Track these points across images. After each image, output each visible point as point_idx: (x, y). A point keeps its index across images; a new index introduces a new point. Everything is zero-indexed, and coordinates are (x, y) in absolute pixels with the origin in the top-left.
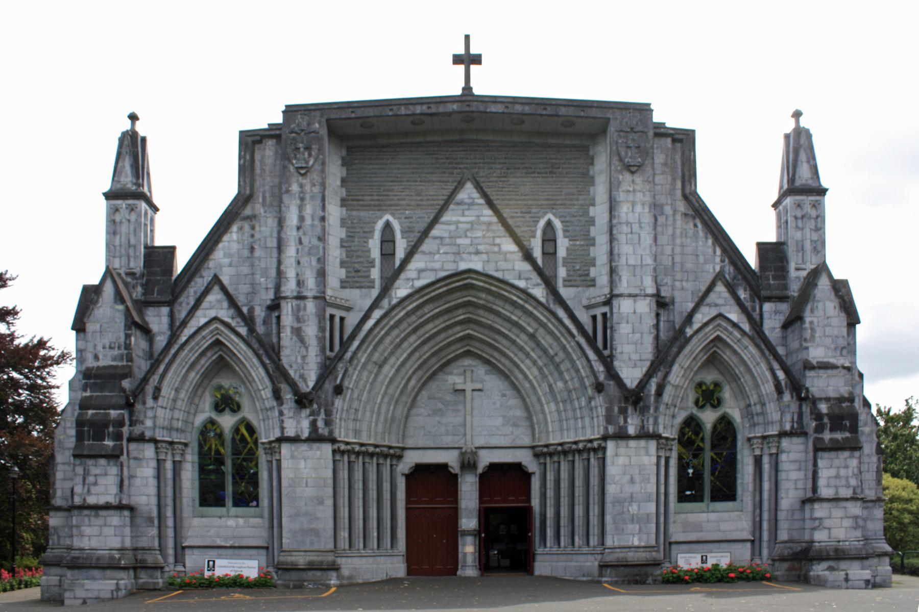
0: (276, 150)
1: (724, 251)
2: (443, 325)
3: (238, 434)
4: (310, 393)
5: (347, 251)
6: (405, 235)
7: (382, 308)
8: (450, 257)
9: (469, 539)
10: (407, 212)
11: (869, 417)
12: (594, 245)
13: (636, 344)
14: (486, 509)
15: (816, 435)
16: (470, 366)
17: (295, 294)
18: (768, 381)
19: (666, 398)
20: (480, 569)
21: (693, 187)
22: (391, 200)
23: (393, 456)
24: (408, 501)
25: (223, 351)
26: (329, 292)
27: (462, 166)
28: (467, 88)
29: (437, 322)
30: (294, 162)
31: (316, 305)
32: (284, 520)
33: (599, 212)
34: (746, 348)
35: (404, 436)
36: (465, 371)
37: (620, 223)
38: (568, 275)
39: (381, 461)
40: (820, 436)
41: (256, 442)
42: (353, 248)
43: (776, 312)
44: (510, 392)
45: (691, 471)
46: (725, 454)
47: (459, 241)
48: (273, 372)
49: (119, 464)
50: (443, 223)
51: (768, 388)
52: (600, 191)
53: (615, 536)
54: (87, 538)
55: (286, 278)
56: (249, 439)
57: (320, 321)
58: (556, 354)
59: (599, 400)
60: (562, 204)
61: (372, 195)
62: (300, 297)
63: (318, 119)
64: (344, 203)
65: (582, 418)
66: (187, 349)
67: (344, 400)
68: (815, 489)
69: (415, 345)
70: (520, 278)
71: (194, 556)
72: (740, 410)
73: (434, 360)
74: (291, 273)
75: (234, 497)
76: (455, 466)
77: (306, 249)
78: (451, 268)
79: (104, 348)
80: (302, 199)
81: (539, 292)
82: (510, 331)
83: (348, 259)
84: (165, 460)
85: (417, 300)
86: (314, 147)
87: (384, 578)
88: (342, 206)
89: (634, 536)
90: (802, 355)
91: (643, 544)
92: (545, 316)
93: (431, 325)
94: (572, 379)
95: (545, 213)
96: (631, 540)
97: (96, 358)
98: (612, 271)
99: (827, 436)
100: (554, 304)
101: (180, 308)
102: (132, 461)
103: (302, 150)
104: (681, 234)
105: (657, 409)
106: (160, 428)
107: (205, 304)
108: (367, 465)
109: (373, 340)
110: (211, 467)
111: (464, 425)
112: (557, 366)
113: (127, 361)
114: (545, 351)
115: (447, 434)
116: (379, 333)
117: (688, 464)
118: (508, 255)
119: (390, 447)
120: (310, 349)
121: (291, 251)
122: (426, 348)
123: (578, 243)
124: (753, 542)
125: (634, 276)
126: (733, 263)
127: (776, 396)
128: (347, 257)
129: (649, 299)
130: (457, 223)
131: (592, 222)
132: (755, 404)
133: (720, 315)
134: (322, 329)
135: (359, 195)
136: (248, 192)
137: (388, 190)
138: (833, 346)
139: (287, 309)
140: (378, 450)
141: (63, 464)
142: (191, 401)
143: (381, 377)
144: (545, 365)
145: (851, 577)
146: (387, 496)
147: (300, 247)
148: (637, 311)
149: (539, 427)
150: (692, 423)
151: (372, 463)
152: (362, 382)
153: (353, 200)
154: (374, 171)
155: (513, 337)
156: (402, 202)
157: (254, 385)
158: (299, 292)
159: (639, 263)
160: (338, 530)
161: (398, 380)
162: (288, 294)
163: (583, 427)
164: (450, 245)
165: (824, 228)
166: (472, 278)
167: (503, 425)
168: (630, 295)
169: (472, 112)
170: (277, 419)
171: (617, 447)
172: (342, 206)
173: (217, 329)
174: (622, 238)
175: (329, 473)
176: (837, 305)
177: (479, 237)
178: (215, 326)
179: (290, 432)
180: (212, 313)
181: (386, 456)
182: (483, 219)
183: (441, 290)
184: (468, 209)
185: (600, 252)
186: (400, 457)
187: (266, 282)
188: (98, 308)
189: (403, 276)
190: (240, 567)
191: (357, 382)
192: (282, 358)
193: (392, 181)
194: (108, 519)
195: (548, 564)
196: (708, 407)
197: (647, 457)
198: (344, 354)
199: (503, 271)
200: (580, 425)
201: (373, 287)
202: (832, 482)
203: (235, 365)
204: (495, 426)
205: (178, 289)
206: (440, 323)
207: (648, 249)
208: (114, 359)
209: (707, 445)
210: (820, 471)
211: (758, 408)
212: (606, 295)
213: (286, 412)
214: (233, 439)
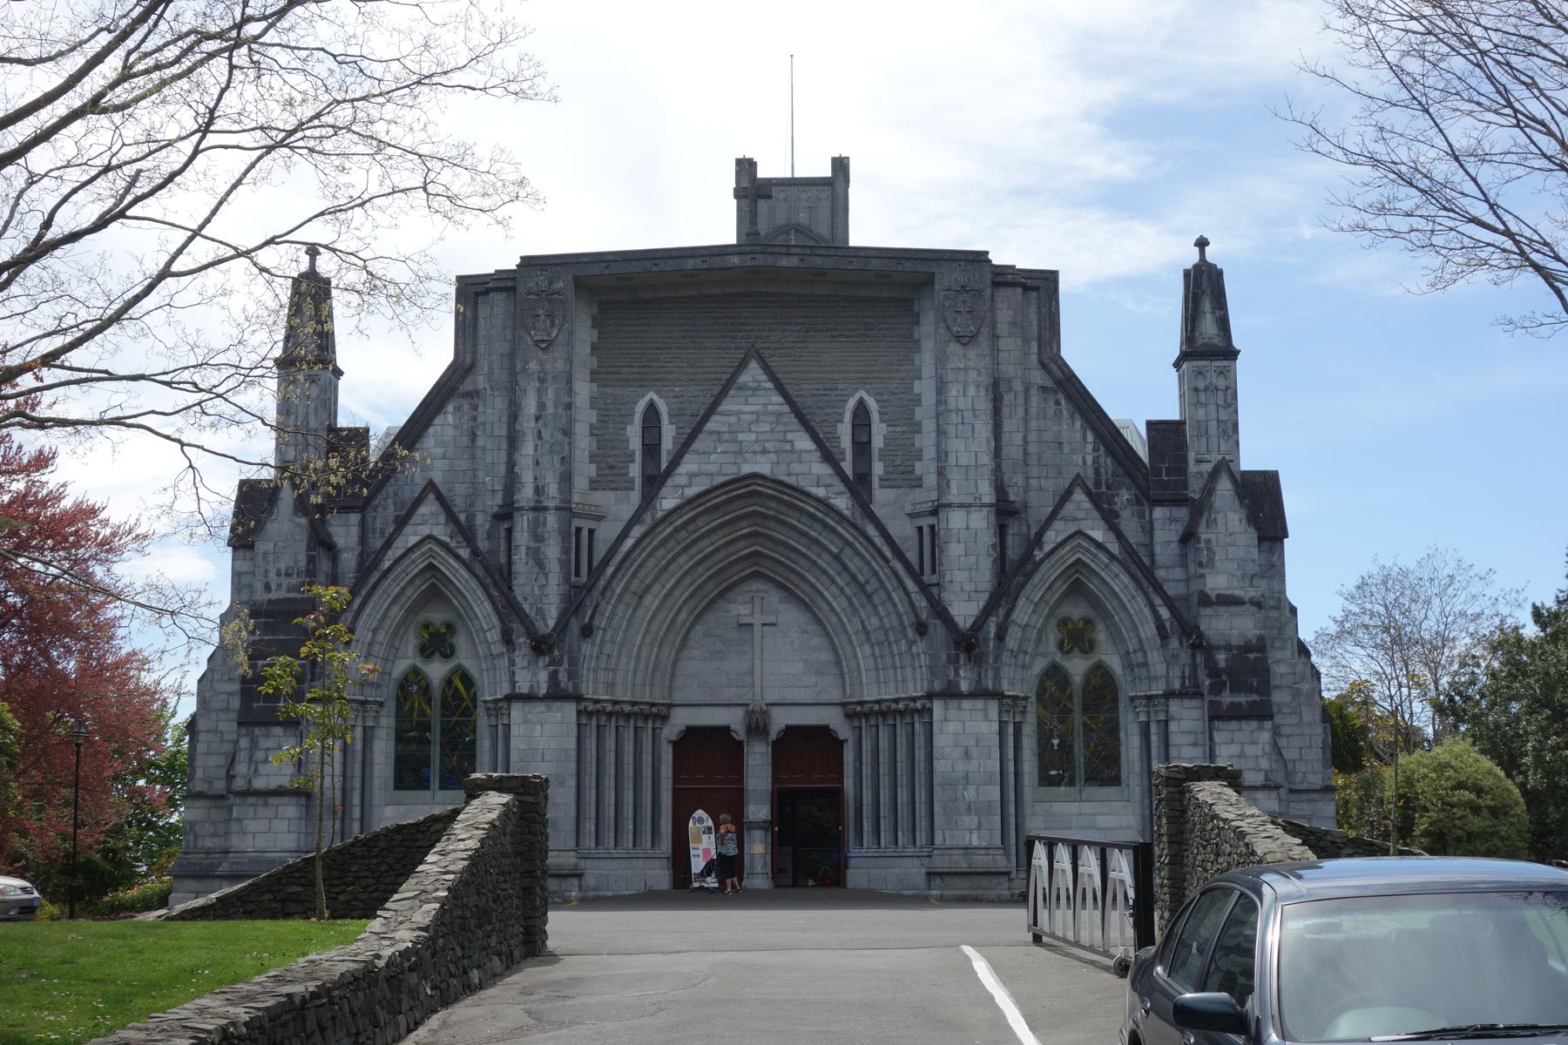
1: (1098, 435)
2: (723, 541)
3: (450, 688)
4: (550, 636)
6: (674, 420)
7: (643, 523)
9: (758, 835)
11: (1308, 668)
12: (920, 432)
13: (969, 570)
17: (532, 504)
18: (1147, 622)
19: (1012, 641)
21: (1055, 350)
23: (656, 717)
24: (676, 778)
26: (576, 498)
27: (747, 328)
29: (714, 537)
33: (925, 388)
34: (1117, 576)
35: (670, 688)
37: (949, 411)
38: (886, 472)
39: (640, 724)
40: (1218, 698)
41: (474, 699)
42: (606, 437)
43: (1171, 520)
44: (812, 628)
47: (741, 437)
48: (503, 607)
49: (298, 733)
51: (1149, 631)
52: (926, 361)
54: (251, 836)
56: (465, 696)
57: (563, 541)
58: (867, 582)
59: (920, 647)
60: (877, 378)
62: (539, 508)
64: (595, 376)
66: (392, 576)
67: (593, 644)
69: (686, 568)
70: (818, 485)
73: (711, 584)
74: (527, 477)
75: (441, 776)
77: (547, 447)
78: (731, 472)
79: (278, 574)
81: (843, 503)
85: (688, 512)
87: (642, 890)
88: (592, 381)
90: (1196, 586)
92: (850, 534)
93: (706, 541)
96: (967, 838)
97: (268, 587)
98: (941, 473)
99: (1227, 698)
105: (997, 658)
107: (415, 519)
108: (621, 729)
109: (632, 564)
112: (869, 597)
114: (854, 577)
116: (639, 555)
119: (653, 705)
121: (527, 448)
122: (700, 570)
123: (899, 429)
125: (967, 479)
126: (1110, 452)
127: (1159, 642)
129: (985, 510)
130: (738, 413)
131: (917, 401)
133: (1079, 533)
134: (566, 551)
136: (468, 360)
138: (1239, 573)
139: (522, 524)
140: (636, 708)
141: (208, 732)
142: (391, 645)
143: (641, 612)
146: (647, 773)
149: (851, 678)
150: (1055, 673)
152: (617, 619)
153: (607, 373)
155: (814, 557)
156: (668, 376)
157: (476, 623)
158: (537, 501)
159: (973, 463)
160: (582, 821)
162: (524, 504)
163: (904, 680)
166: (758, 485)
168: (961, 506)
171: (946, 709)
172: (592, 381)
173: (431, 550)
175: (572, 743)
176: (1244, 517)
179: (523, 688)
180: (425, 530)
181: (646, 717)
182: (770, 408)
183: (718, 500)
185: (926, 441)
186: (665, 718)
187: (492, 481)
189: (670, 482)
191: (610, 619)
194: (280, 808)
196: (1076, 651)
198: (594, 584)
201: (633, 489)
206: (719, 539)
207: (984, 444)
209: (1077, 704)
213: (518, 660)
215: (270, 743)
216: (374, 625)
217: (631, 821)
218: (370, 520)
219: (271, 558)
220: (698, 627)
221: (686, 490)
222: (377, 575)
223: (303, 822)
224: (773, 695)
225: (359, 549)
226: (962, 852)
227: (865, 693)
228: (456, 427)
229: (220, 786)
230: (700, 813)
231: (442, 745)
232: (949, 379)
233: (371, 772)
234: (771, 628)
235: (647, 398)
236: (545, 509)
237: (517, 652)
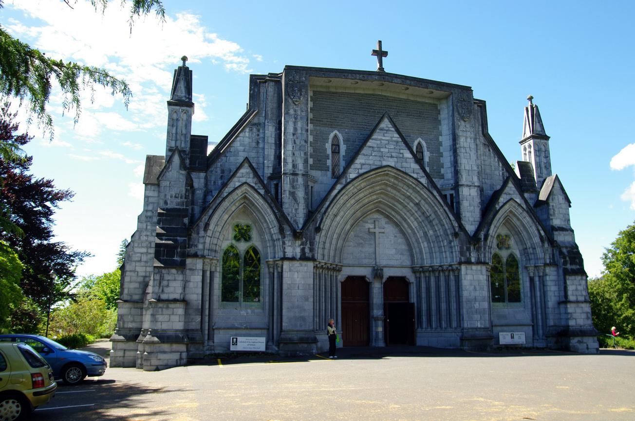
0: (274, 88)
7: (341, 184)
15: (564, 267)
16: (377, 218)
24: (342, 299)
28: (381, 68)
31: (303, 179)
32: (284, 311)
36: (375, 221)
37: (460, 147)
40: (566, 267)
41: (259, 260)
47: (382, 150)
50: (373, 139)
51: (537, 240)
52: (445, 128)
53: (469, 322)
54: (160, 323)
56: (255, 258)
57: (305, 189)
58: (430, 215)
62: (295, 174)
63: (304, 75)
65: (445, 252)
68: (566, 296)
70: (414, 173)
72: (519, 251)
77: (298, 147)
78: (378, 164)
80: (296, 118)
82: (404, 200)
86: (303, 90)
94: (439, 230)
95: (417, 138)
100: (431, 188)
101: (211, 174)
102: (188, 271)
103: (297, 91)
105: (485, 249)
106: (207, 250)
107: (239, 175)
110: (230, 276)
115: (365, 258)
118: (407, 160)
120: (300, 205)
123: (434, 155)
125: (469, 175)
126: (507, 171)
128: (314, 151)
130: (381, 140)
131: (440, 144)
132: (529, 248)
133: (511, 199)
138: (563, 219)
141: (131, 271)
144: (423, 221)
145: (589, 347)
147: (294, 145)
149: (417, 256)
153: (317, 120)
158: (294, 171)
165: (550, 156)
166: (389, 171)
168: (467, 186)
173: (246, 189)
174: (462, 155)
176: (564, 197)
179: (289, 254)
180: (244, 180)
182: (394, 139)
184: (386, 133)
186: (339, 270)
188: (169, 172)
193: (338, 112)
197: (482, 276)
199: (405, 168)
200: (444, 256)
201: (329, 171)
202: (575, 293)
204: (392, 254)
207: (474, 162)
208: (178, 204)
210: (568, 286)
211: (531, 251)
212: (452, 184)
213: (287, 242)
214: (245, 257)
215: (170, 278)
221: (360, 170)
225: (205, 189)
232: (460, 135)
234: (383, 234)
236: (297, 175)
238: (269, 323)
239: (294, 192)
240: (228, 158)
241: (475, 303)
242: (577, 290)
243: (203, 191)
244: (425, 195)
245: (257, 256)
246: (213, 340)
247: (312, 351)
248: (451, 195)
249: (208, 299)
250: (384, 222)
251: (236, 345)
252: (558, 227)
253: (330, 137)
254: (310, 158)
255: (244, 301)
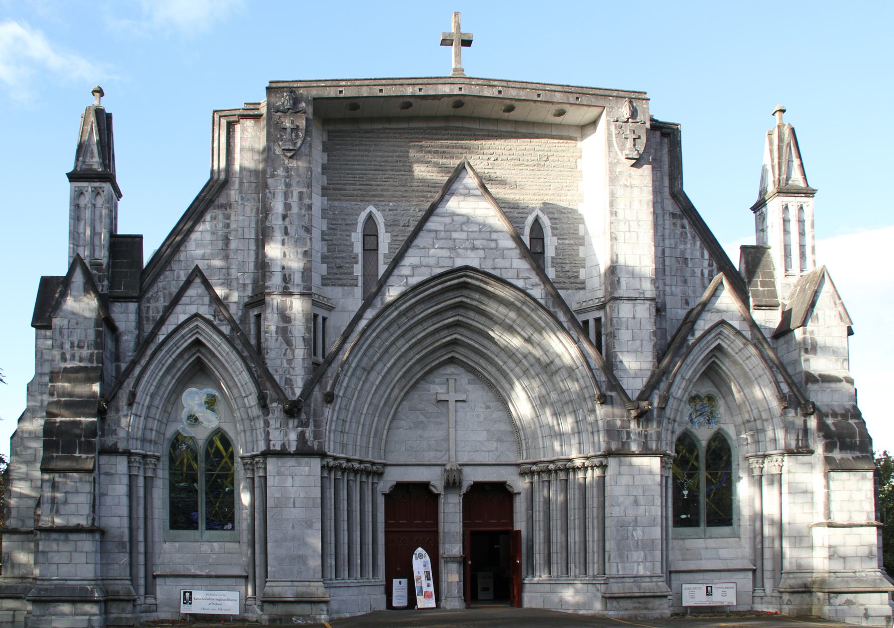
4: (299, 401)
5: (328, 245)
6: (390, 229)
8: (446, 253)
9: (454, 567)
10: (391, 204)
14: (473, 533)
16: (453, 374)
20: (465, 601)
22: (374, 190)
25: (201, 353)
30: (281, 143)
36: (448, 380)
39: (364, 479)
41: (232, 457)
42: (335, 242)
44: (494, 404)
45: (685, 492)
46: (720, 474)
47: (455, 235)
54: (55, 566)
55: (271, 272)
56: (224, 453)
61: (355, 184)
64: (325, 192)
67: (334, 410)
69: (403, 350)
70: (518, 278)
71: (166, 587)
73: (418, 367)
75: (207, 519)
76: (438, 486)
78: (446, 266)
79: (72, 346)
83: (330, 254)
84: (137, 475)
87: (369, 612)
88: (323, 195)
89: (639, 565)
91: (648, 573)
102: (102, 476)
104: (670, 235)
107: (184, 300)
108: (351, 482)
110: (182, 484)
111: (447, 439)
113: (98, 363)
115: (429, 450)
116: (370, 335)
117: (682, 484)
118: (505, 252)
119: (373, 464)
124: (754, 571)
128: (329, 251)
135: (341, 184)
137: (371, 179)
143: (367, 385)
147: (286, 238)
148: (637, 316)
149: (527, 443)
151: (356, 480)
152: (350, 390)
154: (357, 158)
156: (385, 193)
161: (383, 388)
164: (446, 239)
167: (488, 440)
168: (629, 299)
169: (464, 95)
170: (262, 430)
173: (197, 327)
177: (475, 232)
178: (196, 323)
180: (192, 310)
183: (435, 289)
186: (380, 475)
190: (219, 600)
192: (267, 361)
193: (375, 170)
194: (79, 543)
195: (539, 594)
201: (357, 285)
203: (214, 370)
204: (479, 441)
205: (148, 280)
213: (272, 422)
214: (207, 453)
216: (151, 391)
217: (359, 557)
218: (144, 309)
219: (66, 332)
220: (405, 403)
222: (153, 347)
223: (99, 554)
224: (464, 459)
225: (137, 332)
226: (632, 580)
227: (542, 455)
228: (213, 233)
229: (30, 525)
230: (420, 550)
231: (206, 494)
233: (152, 515)
235: (367, 211)
237: (271, 415)
238: (859, 580)
239: (286, 327)
240: (175, 273)
241: (634, 530)
242: (850, 500)
243: (134, 336)
244: (540, 321)
245: (228, 448)
246: (155, 595)
247: (318, 617)
248: (598, 320)
249: (142, 525)
250: (467, 381)
251: (190, 603)
252: (820, 375)
253: (358, 220)
254: (357, 276)
255: (207, 529)
